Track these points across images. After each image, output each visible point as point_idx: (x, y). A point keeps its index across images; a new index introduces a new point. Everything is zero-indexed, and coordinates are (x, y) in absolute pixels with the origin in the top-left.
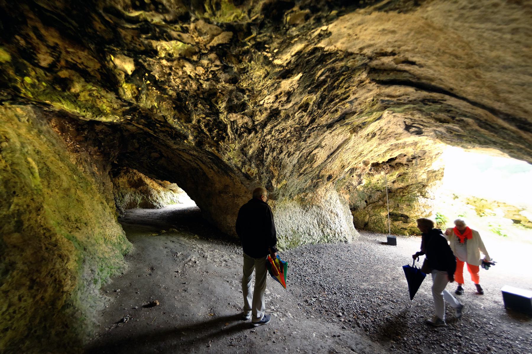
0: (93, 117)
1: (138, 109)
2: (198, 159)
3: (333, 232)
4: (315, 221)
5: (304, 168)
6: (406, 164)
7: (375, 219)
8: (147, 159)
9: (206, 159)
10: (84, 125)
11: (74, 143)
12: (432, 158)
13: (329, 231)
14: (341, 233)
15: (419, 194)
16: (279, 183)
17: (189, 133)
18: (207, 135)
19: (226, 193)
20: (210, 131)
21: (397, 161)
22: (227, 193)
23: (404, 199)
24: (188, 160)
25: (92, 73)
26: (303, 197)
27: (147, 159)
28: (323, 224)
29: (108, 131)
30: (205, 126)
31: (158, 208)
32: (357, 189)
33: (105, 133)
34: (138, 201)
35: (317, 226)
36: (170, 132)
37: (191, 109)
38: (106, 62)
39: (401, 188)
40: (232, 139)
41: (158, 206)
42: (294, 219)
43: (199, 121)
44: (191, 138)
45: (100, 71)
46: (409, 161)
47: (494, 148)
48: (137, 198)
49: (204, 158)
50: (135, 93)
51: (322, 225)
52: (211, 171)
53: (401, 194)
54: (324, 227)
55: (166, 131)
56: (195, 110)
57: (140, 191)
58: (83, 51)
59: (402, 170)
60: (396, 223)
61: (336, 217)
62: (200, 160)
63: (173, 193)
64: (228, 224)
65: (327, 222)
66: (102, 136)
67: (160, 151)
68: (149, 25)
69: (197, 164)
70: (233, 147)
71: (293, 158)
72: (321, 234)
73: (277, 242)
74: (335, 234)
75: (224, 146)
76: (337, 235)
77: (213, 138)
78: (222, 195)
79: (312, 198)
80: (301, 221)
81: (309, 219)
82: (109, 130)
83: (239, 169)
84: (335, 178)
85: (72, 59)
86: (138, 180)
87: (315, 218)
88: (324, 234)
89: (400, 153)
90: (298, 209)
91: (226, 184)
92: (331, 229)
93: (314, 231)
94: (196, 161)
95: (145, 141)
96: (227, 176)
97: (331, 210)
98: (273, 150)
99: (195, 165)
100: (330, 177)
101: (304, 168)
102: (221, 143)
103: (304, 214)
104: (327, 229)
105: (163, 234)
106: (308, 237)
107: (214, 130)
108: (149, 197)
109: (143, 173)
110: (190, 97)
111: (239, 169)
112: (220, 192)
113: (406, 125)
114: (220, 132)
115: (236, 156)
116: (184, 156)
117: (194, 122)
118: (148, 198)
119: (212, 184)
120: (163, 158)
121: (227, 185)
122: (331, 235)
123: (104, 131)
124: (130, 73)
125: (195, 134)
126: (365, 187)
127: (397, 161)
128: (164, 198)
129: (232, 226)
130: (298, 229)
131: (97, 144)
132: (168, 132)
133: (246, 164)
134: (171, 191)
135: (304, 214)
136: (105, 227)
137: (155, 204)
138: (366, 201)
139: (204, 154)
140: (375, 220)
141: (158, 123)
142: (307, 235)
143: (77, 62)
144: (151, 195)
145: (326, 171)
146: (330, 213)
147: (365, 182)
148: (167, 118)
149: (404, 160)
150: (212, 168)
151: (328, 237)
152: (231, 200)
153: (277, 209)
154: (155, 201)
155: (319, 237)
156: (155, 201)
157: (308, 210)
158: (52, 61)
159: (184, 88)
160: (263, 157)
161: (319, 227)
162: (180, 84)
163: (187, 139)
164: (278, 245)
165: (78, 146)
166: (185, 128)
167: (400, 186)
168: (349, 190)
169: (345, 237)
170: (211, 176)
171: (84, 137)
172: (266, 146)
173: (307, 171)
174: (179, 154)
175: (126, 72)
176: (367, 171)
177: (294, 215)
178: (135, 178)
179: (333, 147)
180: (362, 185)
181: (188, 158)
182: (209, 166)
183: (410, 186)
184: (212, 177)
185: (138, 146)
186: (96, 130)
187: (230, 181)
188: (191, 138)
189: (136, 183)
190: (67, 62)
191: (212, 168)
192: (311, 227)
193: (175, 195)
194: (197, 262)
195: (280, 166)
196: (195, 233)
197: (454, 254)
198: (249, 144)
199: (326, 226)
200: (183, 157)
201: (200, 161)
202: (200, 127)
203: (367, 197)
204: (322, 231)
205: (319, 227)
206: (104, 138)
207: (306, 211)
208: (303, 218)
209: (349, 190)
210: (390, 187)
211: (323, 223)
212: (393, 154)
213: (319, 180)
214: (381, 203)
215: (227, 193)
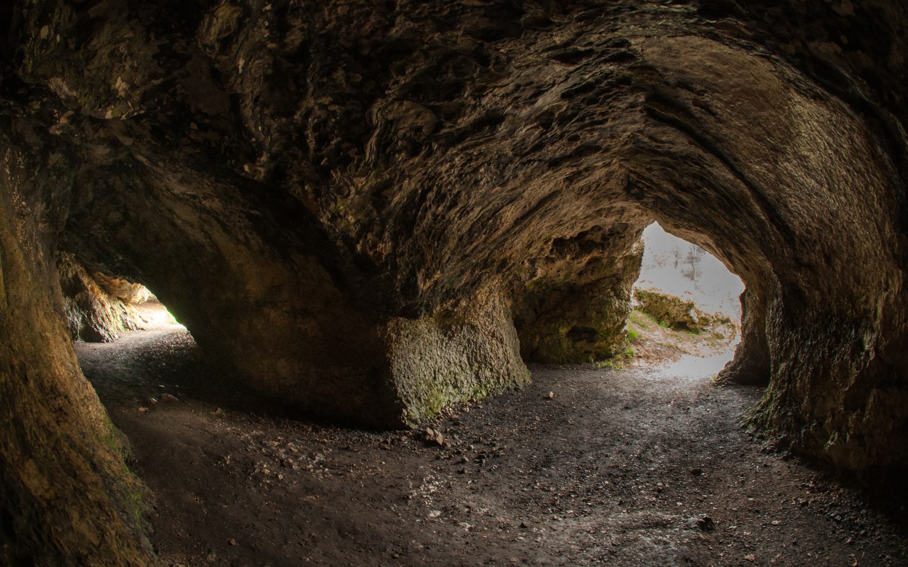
3: (495, 375)
4: (464, 359)
5: (475, 244)
6: (600, 244)
7: (549, 341)
12: (632, 236)
13: (488, 373)
14: (509, 375)
15: (612, 294)
16: (430, 279)
20: (322, 141)
21: (589, 237)
23: (593, 302)
26: (450, 308)
28: (478, 362)
32: (525, 287)
35: (468, 366)
36: (213, 145)
39: (589, 284)
40: (367, 164)
42: (427, 358)
43: (309, 112)
46: (605, 238)
48: (76, 319)
51: (476, 364)
53: (590, 294)
54: (480, 368)
59: (595, 254)
60: (579, 345)
61: (500, 345)
65: (485, 357)
68: (703, 168)
69: (206, 232)
70: (360, 185)
71: (467, 220)
72: (475, 381)
73: (404, 411)
74: (498, 378)
76: (501, 380)
79: (466, 309)
80: (439, 361)
81: (453, 356)
83: (351, 243)
84: (511, 267)
86: (73, 278)
87: (463, 352)
88: (480, 381)
89: (594, 225)
90: (434, 336)
92: (491, 370)
93: (462, 378)
94: (207, 227)
97: (492, 331)
98: (440, 198)
100: (504, 263)
101: (475, 244)
102: (336, 175)
103: (444, 345)
104: (486, 371)
106: (453, 392)
111: (351, 243)
113: (629, 182)
114: (345, 145)
115: (354, 211)
122: (492, 381)
126: (537, 283)
127: (589, 237)
128: (112, 319)
130: (435, 378)
133: (372, 231)
135: (444, 345)
138: (535, 310)
140: (550, 344)
142: (451, 387)
144: (94, 311)
145: (502, 251)
146: (490, 337)
147: (540, 273)
149: (597, 237)
151: (488, 386)
153: (404, 340)
155: (471, 389)
156: (101, 326)
157: (453, 336)
160: (416, 215)
161: (472, 369)
164: (407, 416)
167: (589, 281)
168: (512, 291)
169: (514, 382)
172: (430, 189)
173: (480, 248)
176: (547, 253)
177: (427, 350)
179: (530, 204)
180: (535, 279)
182: (241, 237)
183: (602, 281)
192: (457, 370)
195: (439, 239)
197: (738, 277)
198: (398, 181)
199: (483, 366)
203: (536, 302)
204: (477, 377)
205: (472, 369)
207: (450, 338)
208: (443, 354)
209: (512, 291)
210: (573, 282)
211: (479, 359)
212: (586, 225)
213: (484, 271)
214: (559, 311)
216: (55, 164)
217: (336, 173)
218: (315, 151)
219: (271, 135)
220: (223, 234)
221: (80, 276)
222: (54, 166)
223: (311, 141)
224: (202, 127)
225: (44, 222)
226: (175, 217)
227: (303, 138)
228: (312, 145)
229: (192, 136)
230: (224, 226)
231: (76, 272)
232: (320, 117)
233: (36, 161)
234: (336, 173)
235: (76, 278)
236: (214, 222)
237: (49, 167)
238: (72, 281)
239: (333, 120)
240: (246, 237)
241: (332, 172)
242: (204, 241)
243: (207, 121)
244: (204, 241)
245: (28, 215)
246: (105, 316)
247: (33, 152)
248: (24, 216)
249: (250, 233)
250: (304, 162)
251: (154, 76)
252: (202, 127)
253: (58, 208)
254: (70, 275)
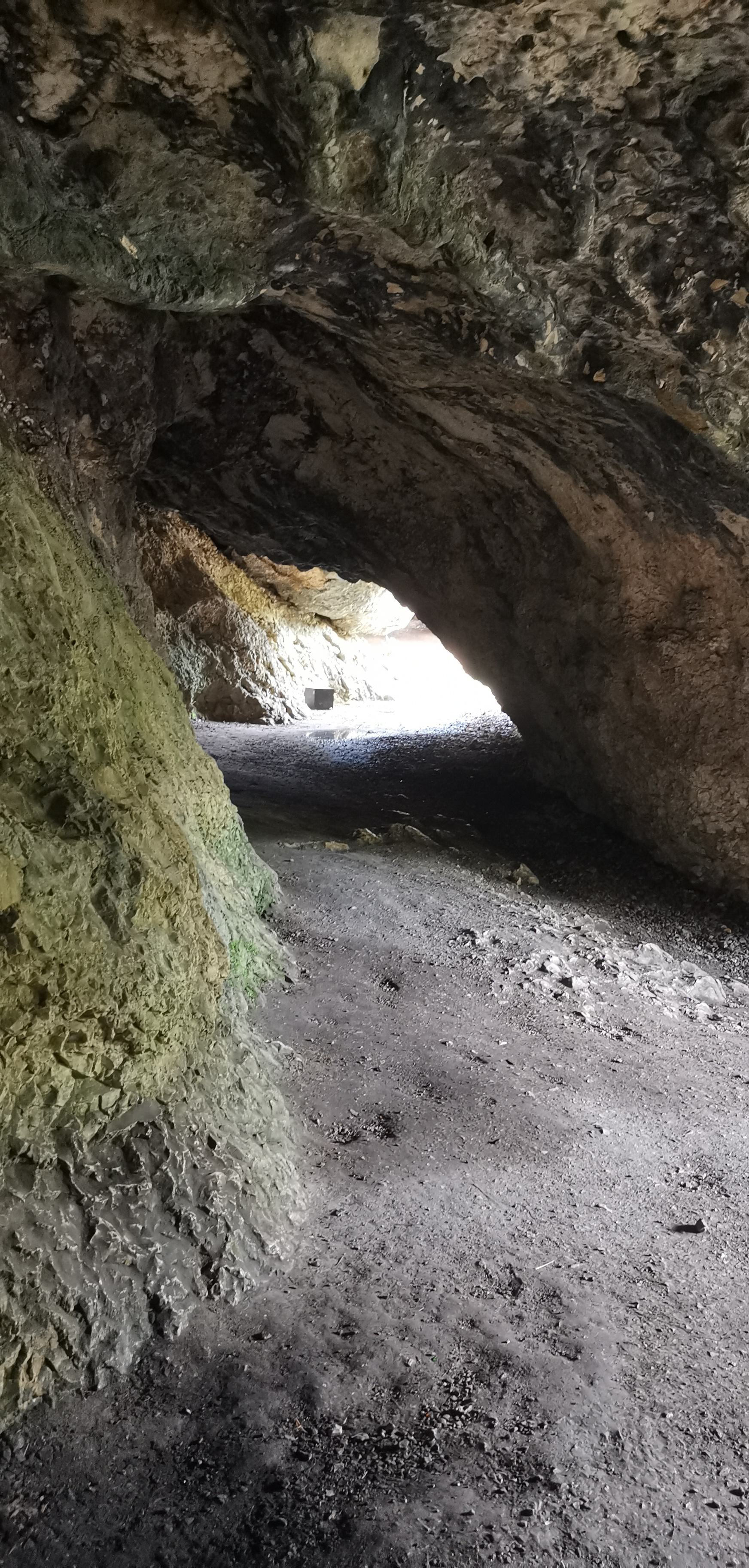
0: (173, 300)
1: (326, 225)
2: (535, 437)
8: (248, 455)
9: (578, 438)
10: (34, 311)
11: (14, 406)
17: (548, 311)
18: (639, 311)
19: (688, 635)
22: (693, 638)
24: (471, 444)
25: (204, 112)
27: (248, 455)
29: (115, 329)
30: (638, 265)
31: (280, 721)
33: (107, 338)
34: (190, 681)
36: (445, 319)
37: (583, 187)
38: (284, 63)
41: (278, 708)
43: (608, 245)
44: (552, 335)
45: (241, 95)
47: (408, 738)
49: (572, 435)
50: (363, 168)
52: (599, 508)
55: (428, 311)
56: (599, 186)
57: (194, 628)
58: (204, 32)
62: (542, 442)
63: (333, 635)
64: (697, 821)
66: (98, 359)
67: (310, 403)
69: (518, 465)
75: (731, 361)
77: (669, 324)
78: (666, 647)
82: (119, 324)
85: (148, 70)
86: (177, 567)
91: (692, 581)
94: (518, 454)
95: (242, 356)
96: (704, 532)
99: (507, 476)
105: (367, 847)
107: (683, 280)
108: (236, 661)
109: (202, 529)
110: (588, 125)
112: (652, 634)
114: (718, 285)
116: (452, 426)
117: (583, 253)
118: (231, 667)
119: (602, 582)
120: (324, 444)
121: (700, 591)
123: (100, 329)
124: (359, 83)
125: (574, 317)
128: (297, 669)
129: (720, 833)
131: (85, 402)
132: (438, 315)
134: (328, 630)
136: (199, 783)
137: (264, 699)
139: (578, 408)
141: (395, 280)
143: (162, 79)
144: (243, 649)
148: (460, 255)
150: (612, 490)
152: (718, 679)
154: (264, 685)
156: (264, 685)
158: (73, 91)
159: (573, 89)
162: (557, 76)
163: (532, 348)
165: (27, 419)
166: (530, 287)
170: (603, 532)
171: (41, 371)
174: (423, 417)
175: (343, 85)
178: (167, 559)
181: (475, 435)
182: (595, 476)
184: (607, 541)
185: (212, 388)
186: (74, 329)
187: (718, 562)
188: (552, 335)
189: (171, 583)
190: (126, 81)
191: (612, 490)
193: (346, 645)
194: (577, 982)
196: (515, 857)
200: (445, 432)
201: (540, 453)
202: (608, 273)
206: (107, 368)
215: (693, 638)
216: (90, 328)
217: (716, 345)
218: (658, 307)
219: (553, 293)
220: (557, 469)
221: (200, 559)
222: (92, 335)
223: (638, 292)
224: (412, 290)
225: (92, 456)
226: (438, 431)
227: (618, 291)
228: (646, 301)
229: (399, 306)
230: (553, 452)
231: (187, 552)
232: (638, 240)
233: (35, 323)
234: (716, 345)
235: (186, 564)
236: (530, 443)
237: (76, 335)
238: (175, 574)
239: (672, 240)
240: (607, 476)
241: (705, 345)
242: (519, 483)
243: (415, 279)
244: (519, 483)
245: (46, 444)
246: (274, 662)
247: (18, 305)
248: (37, 447)
249: (616, 467)
250: (643, 331)
251: (276, 221)
252: (412, 290)
253: (126, 426)
254: (167, 559)
